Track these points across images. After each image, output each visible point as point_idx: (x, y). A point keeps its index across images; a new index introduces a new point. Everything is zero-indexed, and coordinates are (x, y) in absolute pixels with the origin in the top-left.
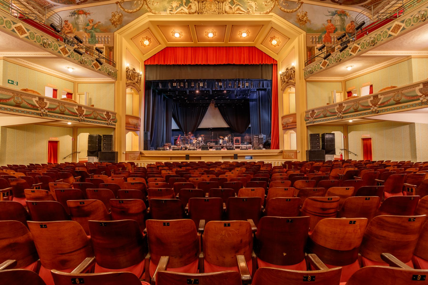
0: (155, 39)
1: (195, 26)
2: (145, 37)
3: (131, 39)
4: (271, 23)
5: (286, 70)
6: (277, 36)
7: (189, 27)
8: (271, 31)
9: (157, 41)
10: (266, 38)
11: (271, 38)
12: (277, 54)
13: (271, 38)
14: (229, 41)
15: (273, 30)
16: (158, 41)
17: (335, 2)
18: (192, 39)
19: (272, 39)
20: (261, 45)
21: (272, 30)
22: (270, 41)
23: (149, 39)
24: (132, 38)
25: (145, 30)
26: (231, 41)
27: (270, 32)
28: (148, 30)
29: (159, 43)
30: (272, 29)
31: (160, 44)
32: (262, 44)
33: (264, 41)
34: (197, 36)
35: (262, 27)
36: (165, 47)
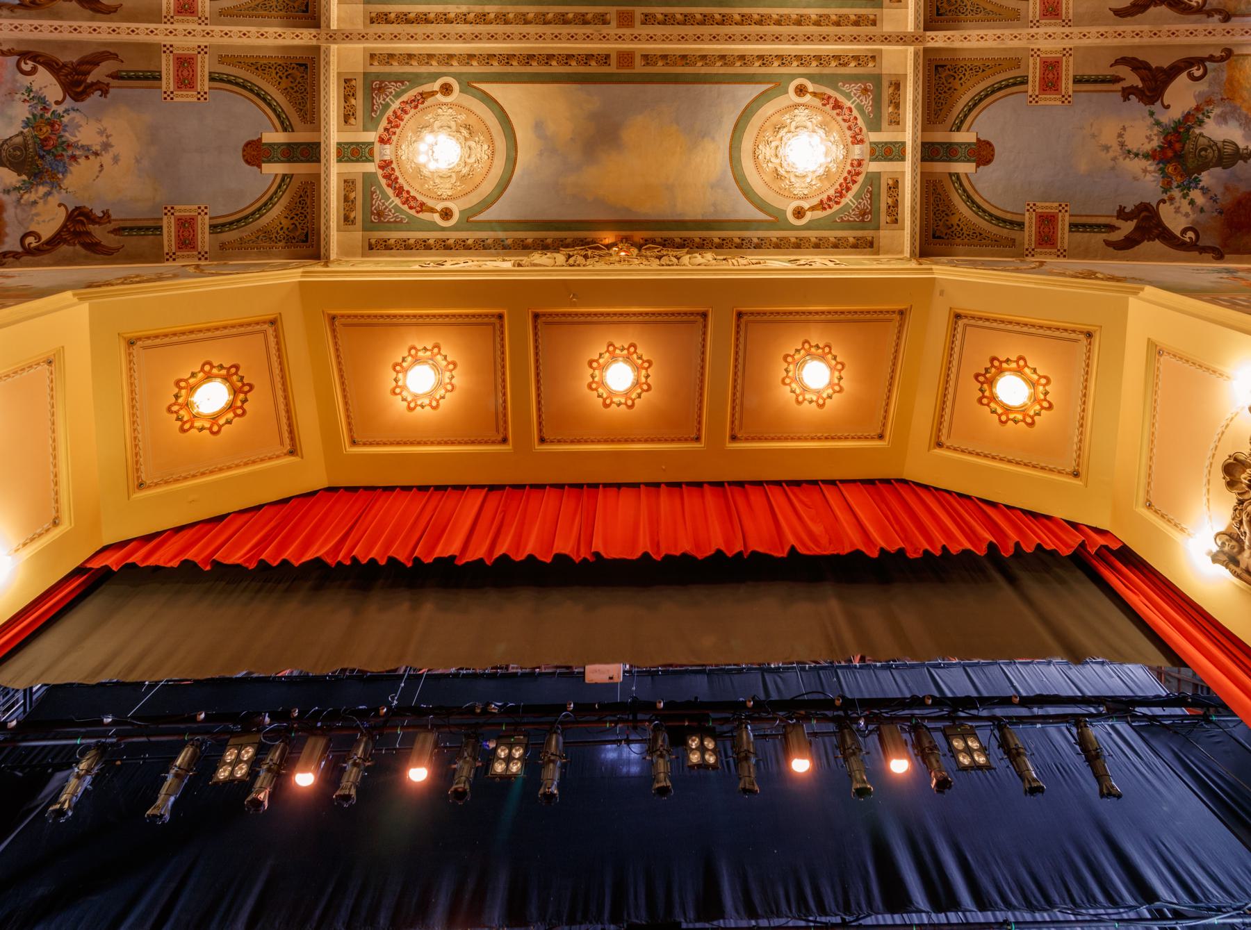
0: (281, 400)
1: (536, 316)
2: (221, 367)
3: (131, 343)
4: (942, 293)
5: (1231, 484)
6: (1008, 350)
7: (502, 326)
8: (959, 336)
9: (284, 421)
10: (951, 390)
11: (977, 376)
12: (1076, 475)
13: (977, 376)
14: (734, 438)
15: (966, 326)
16: (290, 425)
17: (1188, 10)
18: (506, 429)
19: (987, 379)
20: (938, 451)
21: (960, 330)
22: (980, 401)
23: (240, 390)
24: (139, 339)
25: (249, 324)
26: (747, 440)
27: (958, 343)
28: (264, 332)
29: (292, 439)
30: (961, 323)
31: (292, 453)
32: (939, 445)
33: (947, 417)
34: (538, 395)
35: (901, 326)
36: (317, 480)
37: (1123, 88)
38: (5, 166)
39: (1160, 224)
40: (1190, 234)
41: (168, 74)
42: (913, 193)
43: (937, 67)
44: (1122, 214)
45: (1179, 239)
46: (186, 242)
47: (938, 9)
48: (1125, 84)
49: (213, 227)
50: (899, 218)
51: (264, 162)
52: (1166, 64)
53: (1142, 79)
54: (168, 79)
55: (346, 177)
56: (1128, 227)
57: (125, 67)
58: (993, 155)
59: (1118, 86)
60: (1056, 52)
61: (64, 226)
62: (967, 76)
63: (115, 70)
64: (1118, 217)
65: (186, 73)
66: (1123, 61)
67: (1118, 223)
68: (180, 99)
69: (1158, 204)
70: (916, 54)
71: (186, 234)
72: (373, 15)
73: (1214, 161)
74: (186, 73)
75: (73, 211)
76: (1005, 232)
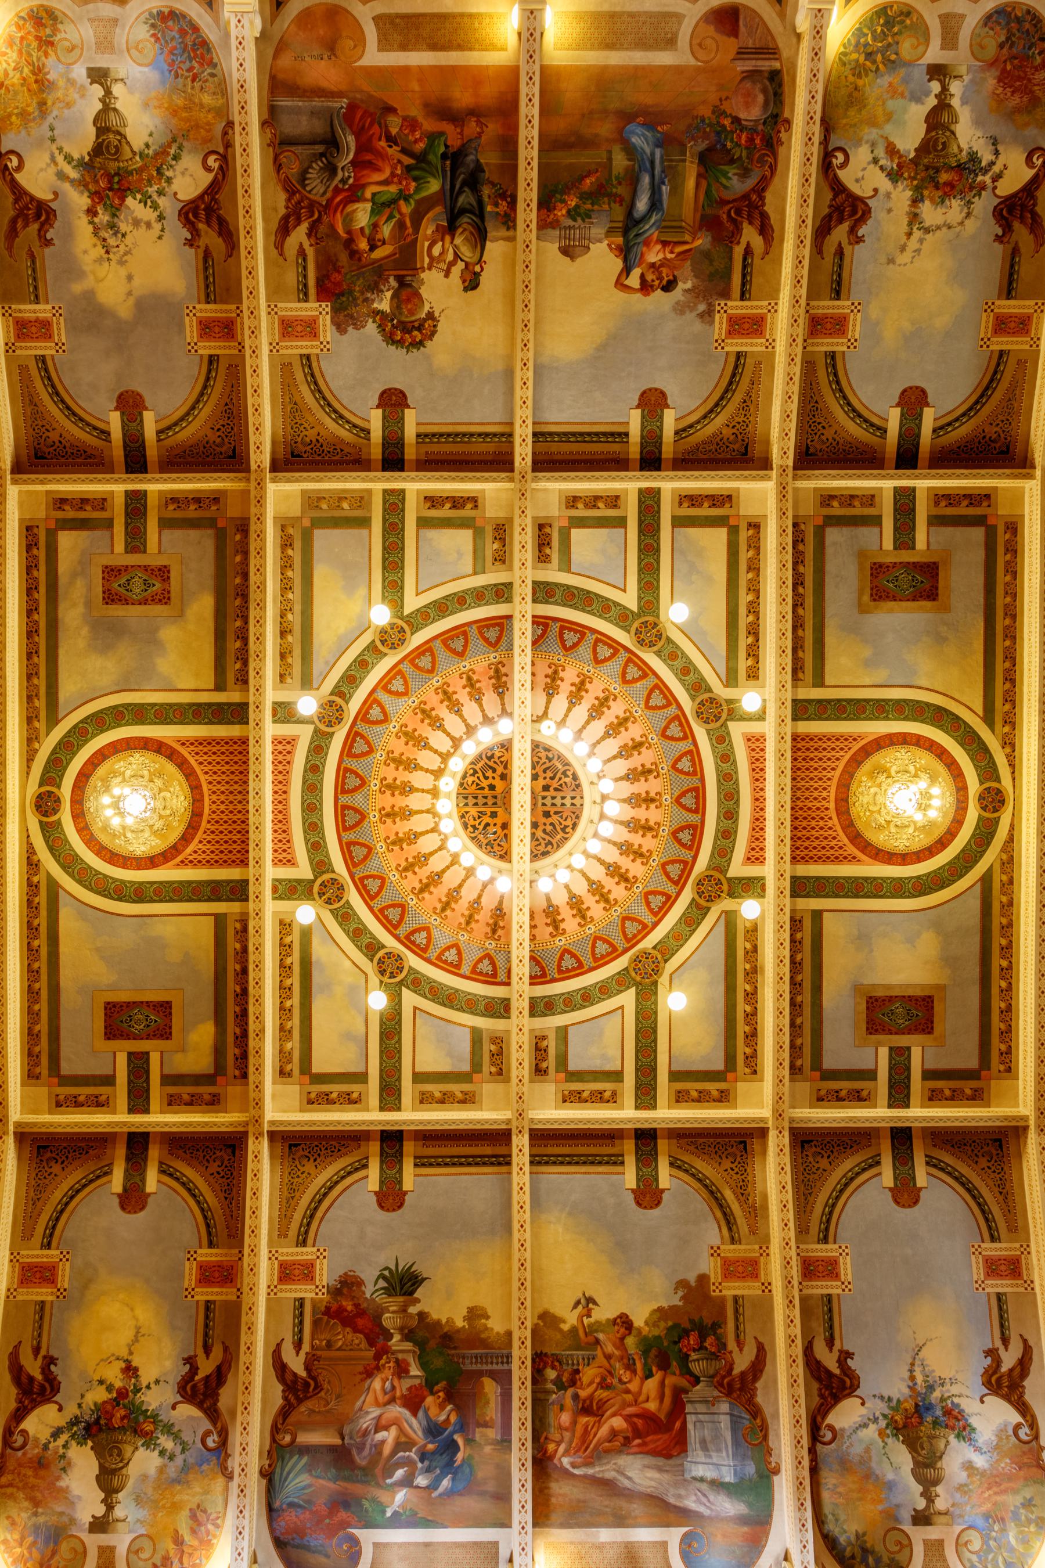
37: (997, 1350)
38: (97, 137)
39: (35, 1404)
40: (20, 1441)
41: (747, 307)
42: (323, 1123)
43: (1000, 1141)
44: (846, 1355)
45: (16, 1427)
46: (1003, 325)
47: (809, 1142)
48: (1002, 1352)
49: (832, 355)
50: (567, 1104)
51: (122, 414)
52: (1028, 1397)
53: (1011, 1370)
54: (742, 308)
55: (622, 498)
56: (830, 1362)
57: (757, 261)
58: (903, 1206)
59: (998, 1344)
60: (766, 1275)
61: (32, 198)
62: (735, 1177)
63: (1023, 250)
64: (841, 1351)
65: (299, 328)
66: (761, 1349)
67: (835, 1355)
68: (984, 319)
69: (56, 1402)
70: (763, 1120)
71: (1012, 325)
72: (803, 527)
73: (107, 1465)
74: (299, 328)
75: (867, 205)
76: (40, 1229)
